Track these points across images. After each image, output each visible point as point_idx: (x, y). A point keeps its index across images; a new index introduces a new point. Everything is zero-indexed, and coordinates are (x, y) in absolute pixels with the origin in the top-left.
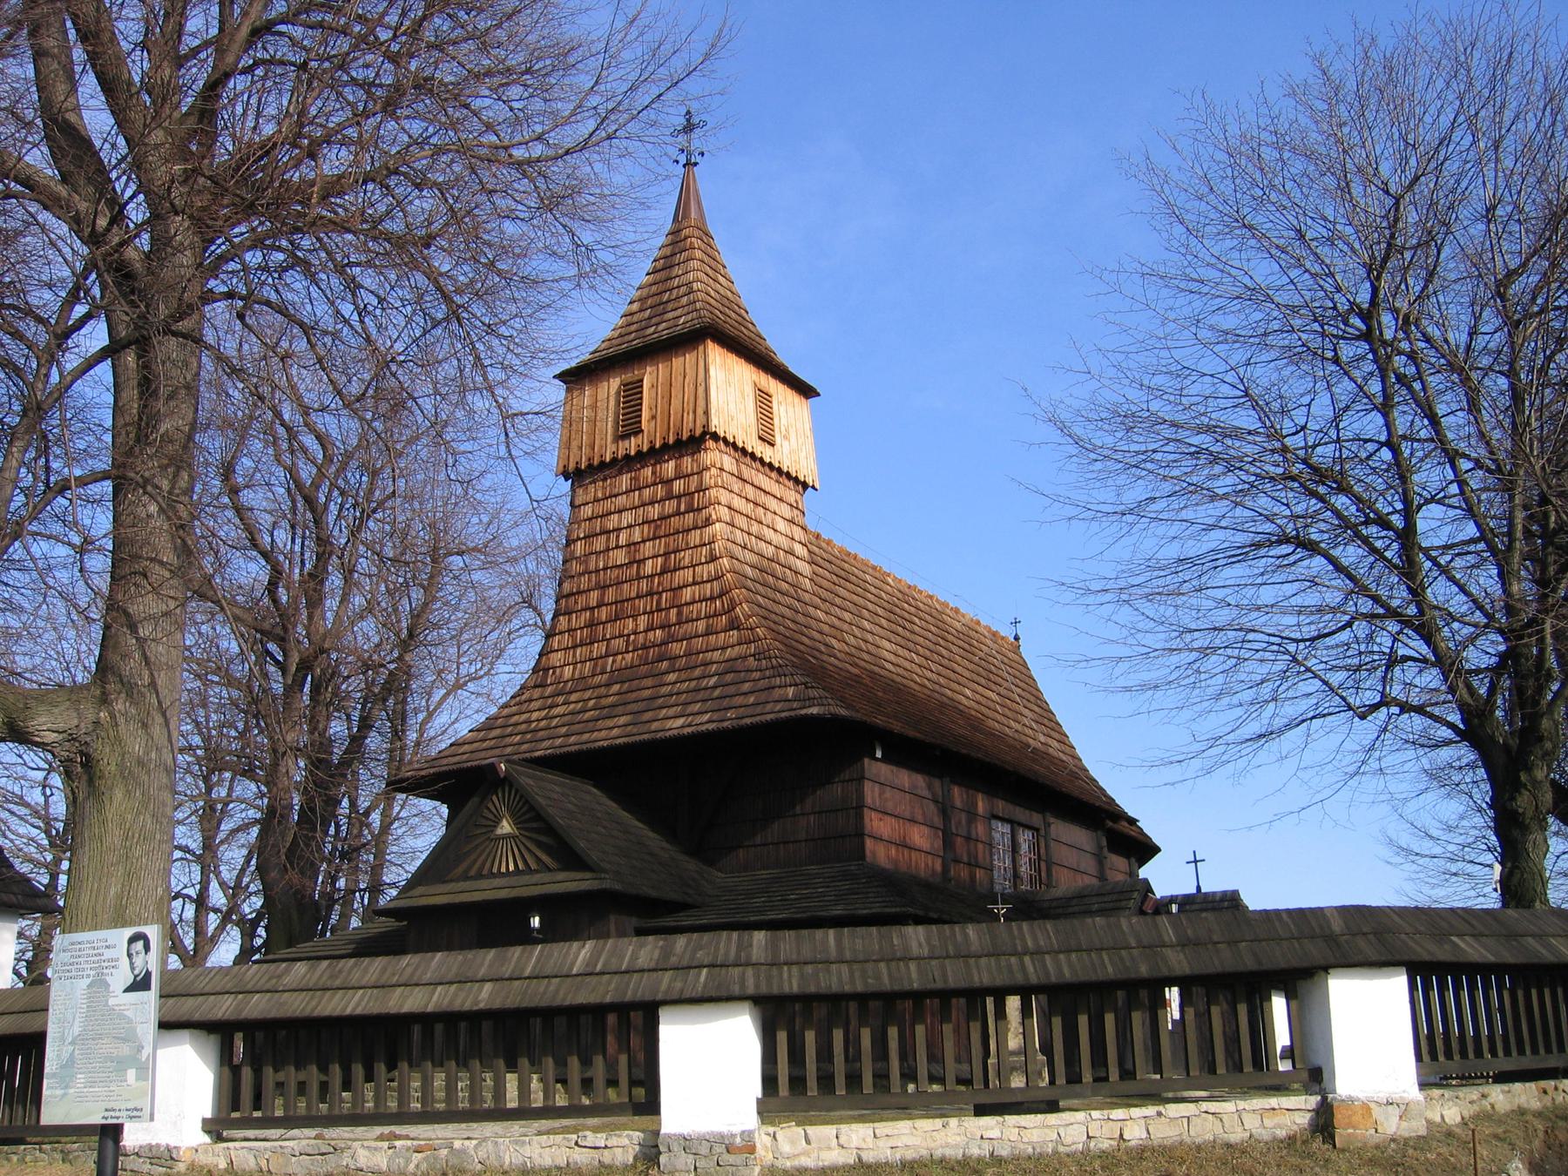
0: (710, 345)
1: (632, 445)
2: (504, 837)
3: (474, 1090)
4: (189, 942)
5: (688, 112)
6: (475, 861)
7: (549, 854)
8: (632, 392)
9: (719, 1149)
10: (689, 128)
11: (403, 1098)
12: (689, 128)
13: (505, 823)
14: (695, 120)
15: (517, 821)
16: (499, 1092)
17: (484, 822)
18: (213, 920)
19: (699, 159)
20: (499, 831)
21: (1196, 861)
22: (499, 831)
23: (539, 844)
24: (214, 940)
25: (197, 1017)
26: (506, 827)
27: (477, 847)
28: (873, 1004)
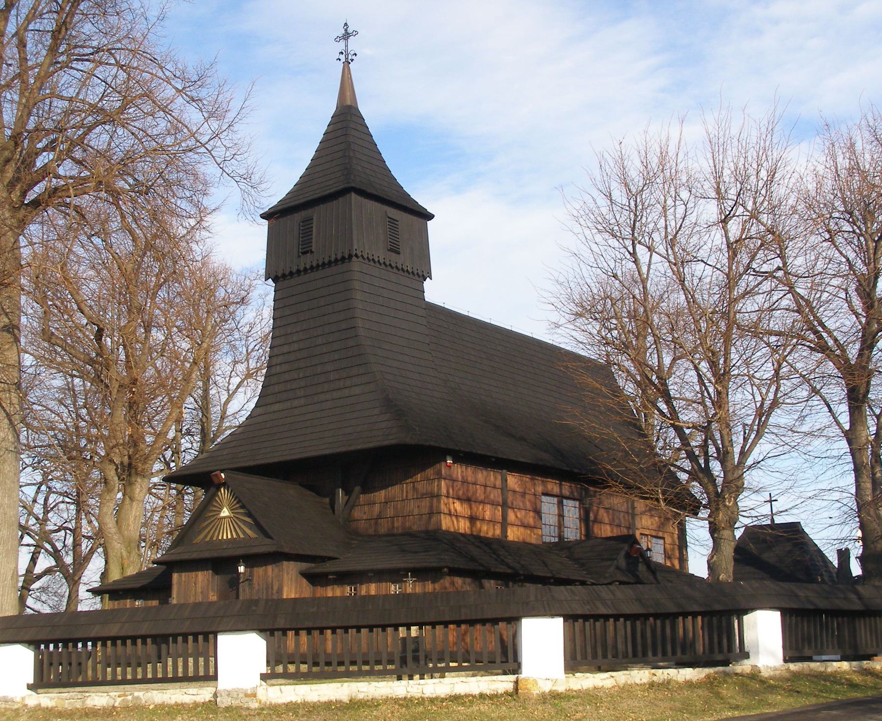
0: (353, 194)
1: (307, 261)
2: (225, 518)
3: (155, 671)
4: (69, 560)
5: (346, 24)
6: (209, 532)
7: (251, 529)
8: (308, 221)
9: (241, 695)
10: (346, 36)
11: (145, 672)
12: (346, 36)
13: (225, 509)
14: (350, 30)
15: (231, 509)
16: (155, 671)
17: (215, 509)
18: (85, 546)
19: (354, 57)
20: (222, 515)
21: (771, 501)
22: (222, 515)
23: (244, 522)
24: (87, 558)
25: (261, 460)
26: (225, 512)
27: (210, 523)
28: (338, 631)
